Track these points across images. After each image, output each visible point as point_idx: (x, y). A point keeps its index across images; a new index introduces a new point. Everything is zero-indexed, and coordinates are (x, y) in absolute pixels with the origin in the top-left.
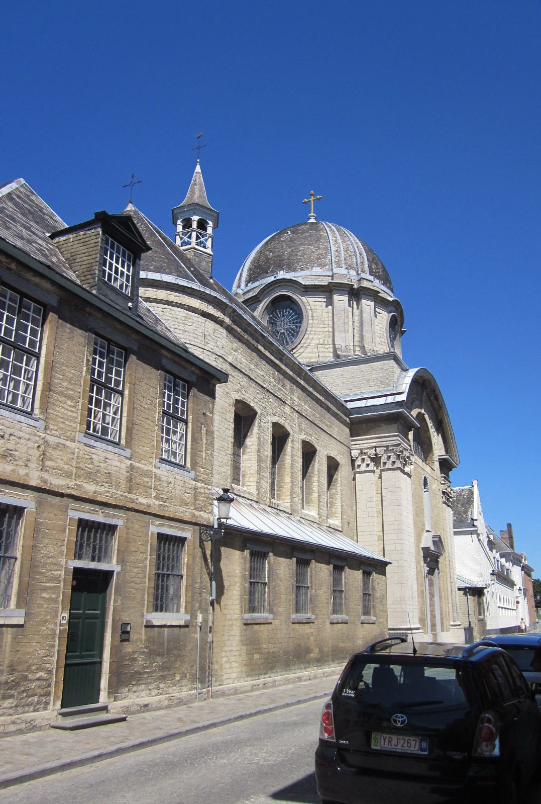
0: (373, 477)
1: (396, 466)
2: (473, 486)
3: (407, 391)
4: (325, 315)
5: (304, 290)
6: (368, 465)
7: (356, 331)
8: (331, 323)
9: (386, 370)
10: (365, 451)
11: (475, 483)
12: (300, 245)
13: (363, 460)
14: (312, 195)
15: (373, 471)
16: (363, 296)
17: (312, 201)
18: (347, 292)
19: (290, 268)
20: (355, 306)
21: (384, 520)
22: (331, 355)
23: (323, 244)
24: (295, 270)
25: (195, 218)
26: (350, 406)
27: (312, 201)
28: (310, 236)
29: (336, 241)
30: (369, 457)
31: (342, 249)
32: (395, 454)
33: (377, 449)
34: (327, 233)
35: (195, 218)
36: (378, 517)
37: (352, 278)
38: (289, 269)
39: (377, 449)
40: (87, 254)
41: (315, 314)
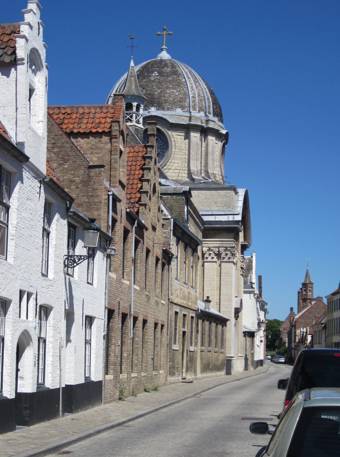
0: (216, 266)
1: (231, 260)
2: (252, 257)
3: (241, 214)
4: (183, 146)
5: (170, 126)
6: (213, 258)
7: (203, 158)
8: (187, 152)
9: (228, 197)
10: (212, 249)
11: (254, 254)
12: (167, 88)
13: (210, 254)
14: (165, 29)
15: (216, 262)
16: (209, 133)
17: (165, 35)
18: (199, 131)
19: (160, 106)
20: (203, 140)
21: (221, 293)
22: (186, 175)
23: (183, 90)
24: (163, 109)
25: (135, 104)
26: (205, 218)
27: (165, 35)
28: (173, 81)
29: (192, 87)
30: (214, 253)
31: (197, 96)
32: (231, 252)
33: (220, 248)
34: (185, 78)
35: (135, 104)
36: (217, 290)
37: (202, 118)
38: (159, 107)
39: (220, 248)
40: (178, 207)
41: (177, 145)
